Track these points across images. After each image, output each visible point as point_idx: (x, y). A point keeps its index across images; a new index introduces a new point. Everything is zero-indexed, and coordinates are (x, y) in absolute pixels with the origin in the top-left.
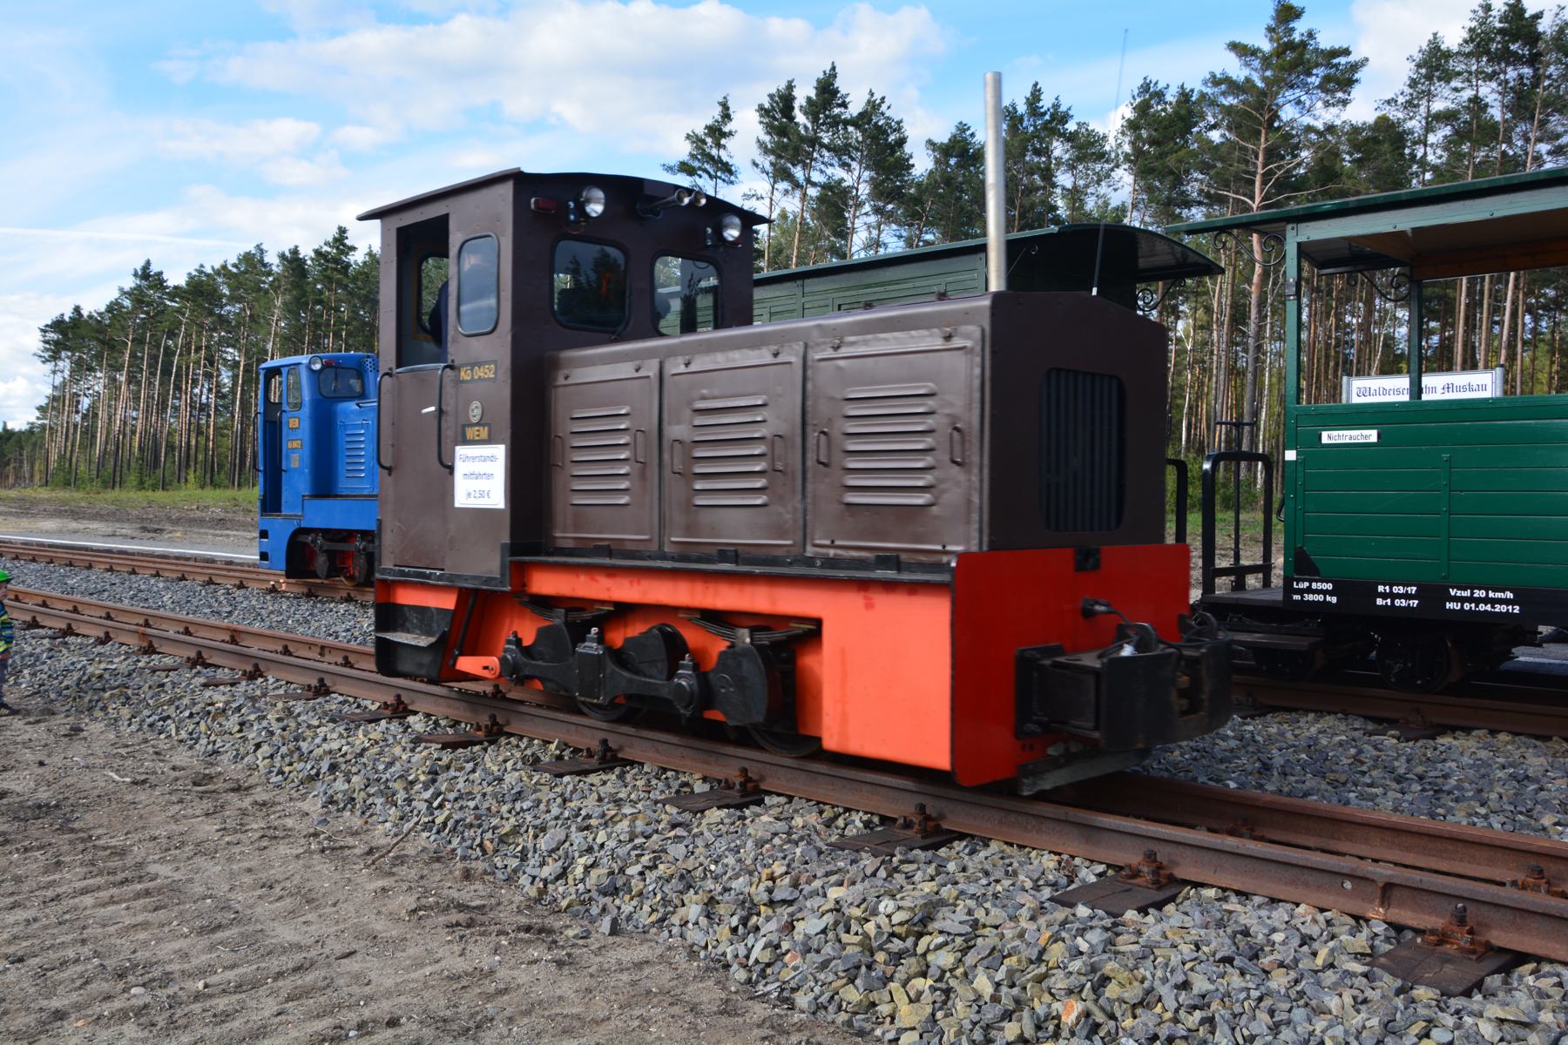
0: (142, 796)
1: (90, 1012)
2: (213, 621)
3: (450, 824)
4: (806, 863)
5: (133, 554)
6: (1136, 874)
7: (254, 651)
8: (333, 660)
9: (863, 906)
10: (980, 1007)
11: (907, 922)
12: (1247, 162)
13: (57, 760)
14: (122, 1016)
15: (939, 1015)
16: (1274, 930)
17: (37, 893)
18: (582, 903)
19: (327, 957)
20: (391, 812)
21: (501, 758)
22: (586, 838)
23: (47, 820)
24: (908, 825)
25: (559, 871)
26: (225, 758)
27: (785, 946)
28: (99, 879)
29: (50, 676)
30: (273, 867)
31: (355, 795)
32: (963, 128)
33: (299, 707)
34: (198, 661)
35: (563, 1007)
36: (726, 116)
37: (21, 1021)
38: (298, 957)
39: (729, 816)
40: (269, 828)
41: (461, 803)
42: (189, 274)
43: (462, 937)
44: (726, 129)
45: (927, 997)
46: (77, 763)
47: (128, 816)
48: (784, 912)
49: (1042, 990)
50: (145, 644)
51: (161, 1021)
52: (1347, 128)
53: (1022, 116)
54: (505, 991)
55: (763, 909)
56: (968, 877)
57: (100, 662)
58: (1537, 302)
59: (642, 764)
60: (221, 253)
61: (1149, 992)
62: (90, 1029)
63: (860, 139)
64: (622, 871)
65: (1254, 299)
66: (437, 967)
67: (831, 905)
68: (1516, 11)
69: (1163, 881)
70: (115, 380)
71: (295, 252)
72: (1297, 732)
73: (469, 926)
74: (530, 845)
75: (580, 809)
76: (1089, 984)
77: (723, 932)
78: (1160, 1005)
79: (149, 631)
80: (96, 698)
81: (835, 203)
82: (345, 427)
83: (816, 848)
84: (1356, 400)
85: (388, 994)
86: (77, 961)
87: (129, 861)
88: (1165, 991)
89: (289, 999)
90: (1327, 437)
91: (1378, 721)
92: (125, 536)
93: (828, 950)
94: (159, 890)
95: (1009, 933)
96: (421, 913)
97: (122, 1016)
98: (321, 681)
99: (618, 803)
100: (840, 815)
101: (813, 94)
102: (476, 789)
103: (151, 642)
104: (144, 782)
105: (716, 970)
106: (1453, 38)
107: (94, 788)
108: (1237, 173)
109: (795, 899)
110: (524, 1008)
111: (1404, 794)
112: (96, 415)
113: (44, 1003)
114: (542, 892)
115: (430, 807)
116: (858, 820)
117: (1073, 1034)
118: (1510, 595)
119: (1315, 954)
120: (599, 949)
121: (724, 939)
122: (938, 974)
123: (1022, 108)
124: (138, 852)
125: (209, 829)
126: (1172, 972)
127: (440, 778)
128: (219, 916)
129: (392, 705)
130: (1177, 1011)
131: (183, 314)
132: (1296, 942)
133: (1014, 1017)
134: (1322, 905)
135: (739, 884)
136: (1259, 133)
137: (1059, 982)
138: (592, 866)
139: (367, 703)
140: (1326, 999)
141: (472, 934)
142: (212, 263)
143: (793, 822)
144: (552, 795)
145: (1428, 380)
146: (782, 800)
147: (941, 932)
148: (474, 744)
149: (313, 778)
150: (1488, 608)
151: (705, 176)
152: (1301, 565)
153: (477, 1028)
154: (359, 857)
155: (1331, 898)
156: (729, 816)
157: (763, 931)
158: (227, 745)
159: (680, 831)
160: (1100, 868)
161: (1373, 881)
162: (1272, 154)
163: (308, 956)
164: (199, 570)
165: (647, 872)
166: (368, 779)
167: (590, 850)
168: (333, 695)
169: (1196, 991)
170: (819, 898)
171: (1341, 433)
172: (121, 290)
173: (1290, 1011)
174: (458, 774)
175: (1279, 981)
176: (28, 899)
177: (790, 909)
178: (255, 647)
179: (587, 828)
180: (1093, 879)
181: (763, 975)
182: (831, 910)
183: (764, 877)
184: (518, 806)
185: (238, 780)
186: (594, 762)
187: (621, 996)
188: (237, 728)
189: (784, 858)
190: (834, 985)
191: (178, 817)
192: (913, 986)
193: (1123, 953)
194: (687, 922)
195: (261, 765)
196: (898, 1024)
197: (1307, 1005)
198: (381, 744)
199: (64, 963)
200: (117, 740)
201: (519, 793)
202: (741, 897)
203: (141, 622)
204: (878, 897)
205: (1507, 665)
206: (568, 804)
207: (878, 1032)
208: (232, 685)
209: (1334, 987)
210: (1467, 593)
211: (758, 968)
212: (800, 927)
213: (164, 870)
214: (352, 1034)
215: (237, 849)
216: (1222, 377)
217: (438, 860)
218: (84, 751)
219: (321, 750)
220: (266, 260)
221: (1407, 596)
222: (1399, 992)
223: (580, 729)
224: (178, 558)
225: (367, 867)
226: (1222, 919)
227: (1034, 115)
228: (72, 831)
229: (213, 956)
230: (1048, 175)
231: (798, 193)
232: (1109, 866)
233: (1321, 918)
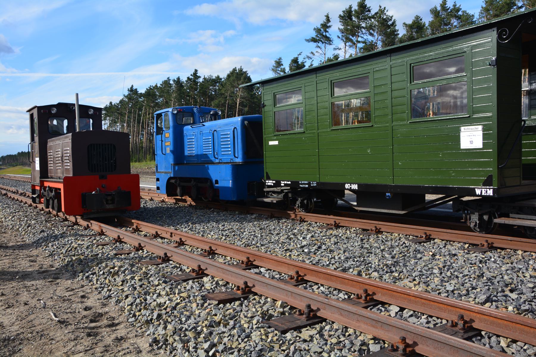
32: (417, 17)
42: (147, 89)
44: (329, 25)
60: (158, 81)
71: (179, 78)
101: (357, 8)
123: (439, 8)
131: (144, 103)
148: (235, 300)
168: (171, 262)
172: (124, 95)
188: (121, 283)
223: (293, 295)
227: (444, 10)
231: (354, 46)
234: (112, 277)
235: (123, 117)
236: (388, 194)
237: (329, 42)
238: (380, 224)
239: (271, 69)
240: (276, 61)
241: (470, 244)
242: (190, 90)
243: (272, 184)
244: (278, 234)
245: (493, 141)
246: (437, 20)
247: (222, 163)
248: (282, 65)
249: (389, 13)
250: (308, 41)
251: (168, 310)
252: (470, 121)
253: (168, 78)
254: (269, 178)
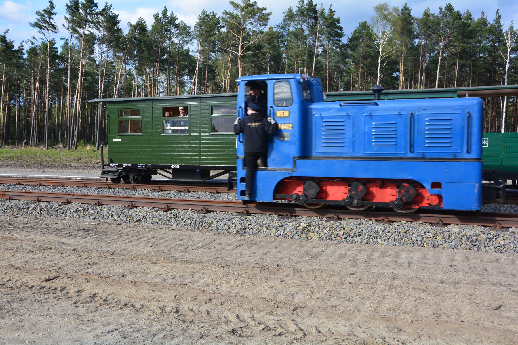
32: (141, 20)
44: (52, 12)
53: (161, 18)
68: (310, 4)
81: (90, 41)
106: (295, 10)
123: (161, 15)
151: (45, 29)
162: (243, 39)
236: (197, 170)
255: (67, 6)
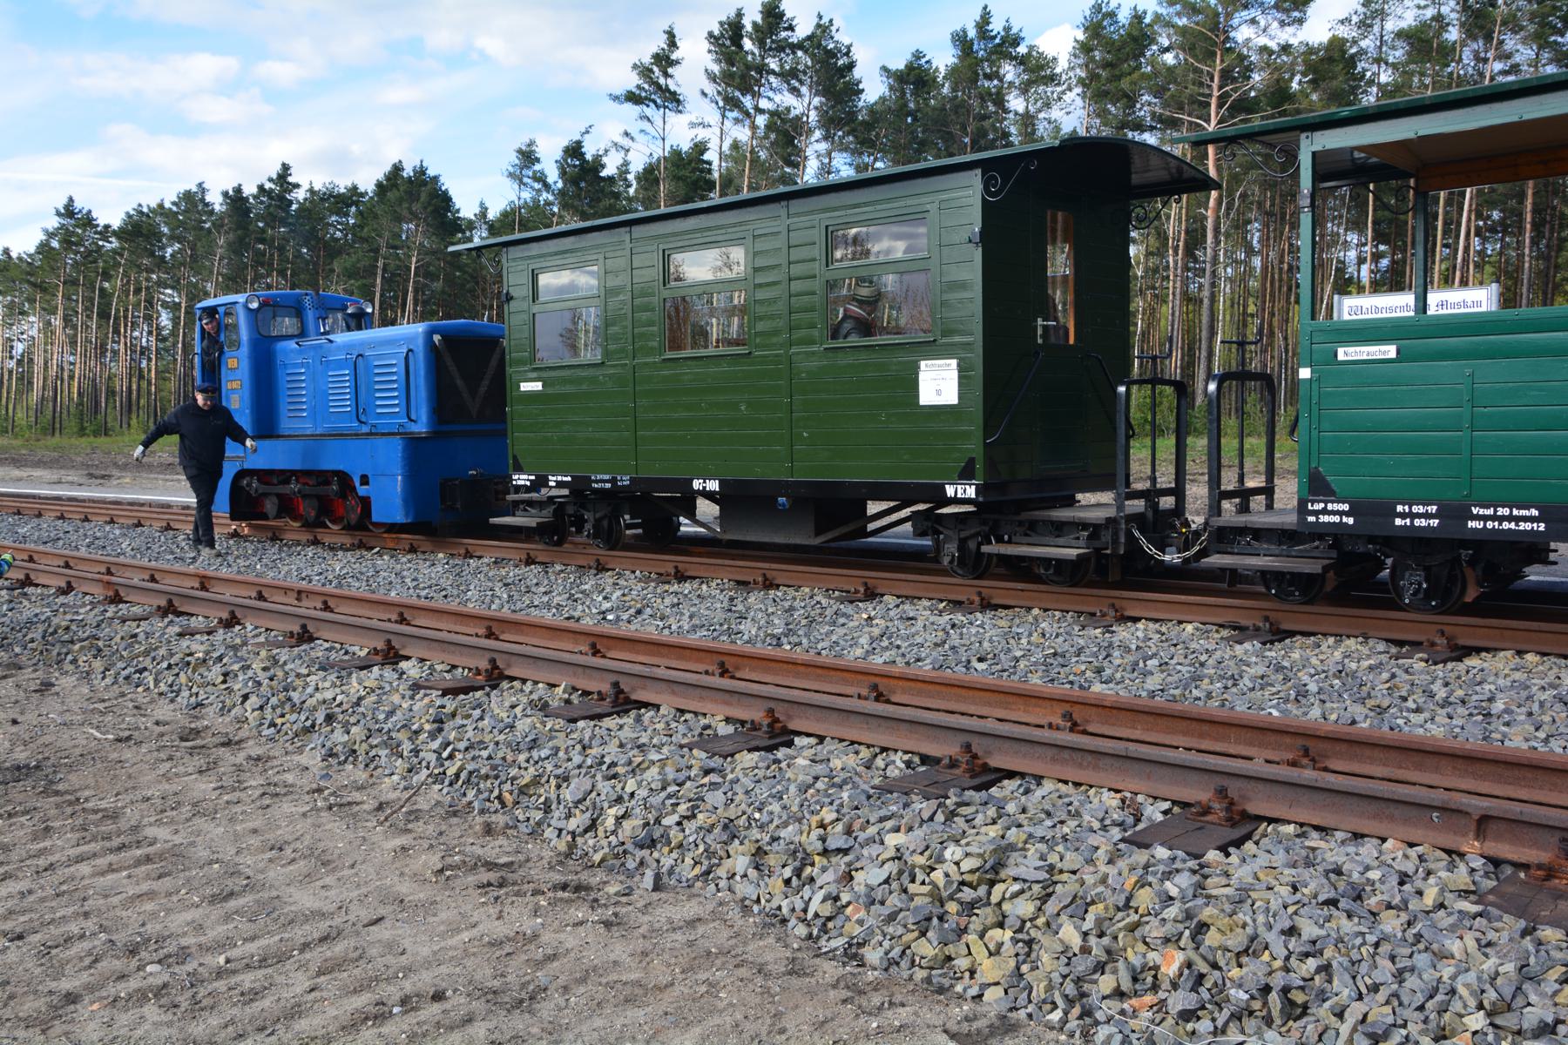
0: (128, 754)
1: (105, 994)
2: (177, 567)
3: (463, 776)
4: (857, 808)
5: (84, 501)
6: (1206, 810)
7: (227, 598)
8: (311, 604)
9: (927, 853)
10: (1069, 959)
11: (978, 869)
12: (1201, 84)
13: (30, 718)
14: (141, 997)
15: (1025, 968)
16: (1368, 868)
17: (28, 862)
18: (617, 856)
19: (354, 924)
20: (397, 764)
21: (507, 704)
22: (614, 787)
23: (29, 783)
24: (953, 764)
25: (588, 822)
26: (210, 711)
27: (845, 898)
28: (93, 845)
29: (12, 629)
30: (279, 827)
31: (356, 747)
32: (918, 55)
33: (284, 654)
34: (169, 610)
35: (620, 973)
36: (672, 44)
37: (30, 1006)
38: (323, 926)
39: (762, 760)
40: (269, 784)
41: (473, 753)
42: (127, 213)
43: (497, 899)
44: (674, 57)
45: (1008, 949)
46: (54, 720)
47: (115, 776)
48: (841, 862)
49: (1136, 940)
50: (111, 593)
51: (184, 1000)
52: (1303, 49)
53: (972, 40)
54: (552, 958)
55: (817, 859)
56: (1031, 819)
57: (65, 613)
58: (1485, 224)
59: (657, 707)
60: (167, 194)
61: (1253, 939)
62: (107, 1012)
63: (809, 63)
64: (658, 821)
65: (1210, 224)
66: (475, 932)
67: (891, 853)
69: (1237, 817)
70: (49, 323)
71: (238, 190)
72: (1321, 657)
73: (501, 886)
74: (553, 796)
75: (603, 756)
76: (1187, 933)
77: (776, 884)
78: (1267, 952)
79: (113, 579)
80: (65, 650)
81: (786, 132)
82: (285, 365)
83: (863, 791)
84: (1346, 317)
85: (427, 964)
86: (82, 936)
87: (123, 824)
88: (1272, 938)
89: (320, 973)
90: (1343, 354)
91: (1400, 643)
92: (72, 483)
93: (894, 901)
94: (161, 856)
95: (1090, 879)
96: (448, 873)
97: (141, 997)
98: (304, 627)
99: (641, 747)
100: (876, 755)
101: (759, 19)
102: (487, 738)
103: (117, 591)
104: (129, 738)
105: (773, 925)
107: (75, 746)
108: (1191, 96)
109: (851, 847)
110: (578, 975)
111: (1451, 718)
112: (31, 361)
113: (53, 985)
114: (572, 846)
115: (439, 758)
116: (899, 759)
117: (1175, 986)
118: (1535, 512)
119: (1420, 893)
120: (645, 906)
121: (777, 891)
122: (1018, 924)
123: (972, 33)
124: (131, 816)
125: (204, 787)
126: (1274, 916)
127: (446, 726)
128: (229, 882)
129: (382, 650)
130: (1287, 958)
131: (121, 255)
132: (1394, 880)
133: (1108, 968)
134: (1411, 839)
135: (788, 833)
136: (1214, 54)
137: (1154, 930)
138: (623, 817)
139: (356, 649)
140: (1447, 942)
141: (507, 894)
142: (150, 201)
143: (831, 765)
144: (570, 743)
145: (1433, 298)
146: (813, 741)
147: (1015, 879)
149: (310, 730)
150: (1513, 526)
152: (1317, 486)
153: (531, 999)
154: (369, 813)
155: (1420, 832)
156: (762, 760)
157: (819, 883)
158: (212, 698)
159: (714, 778)
160: (1166, 805)
161: (1467, 813)
162: (1226, 76)
163: (334, 924)
164: (155, 516)
165: (685, 822)
166: (369, 730)
167: (619, 800)
168: (318, 642)
169: (1305, 937)
170: (876, 846)
171: (1358, 349)
173: (1411, 956)
174: (465, 722)
175: (1391, 924)
176: (19, 869)
177: (847, 859)
178: (227, 593)
179: (615, 776)
180: (1160, 817)
181: (824, 929)
182: (893, 859)
183: (814, 825)
184: (535, 754)
185: (227, 734)
186: (606, 706)
187: (681, 958)
188: (221, 678)
189: (831, 804)
190: (905, 938)
191: (169, 775)
192: (991, 938)
193: (1216, 898)
194: (734, 874)
195: (250, 718)
196: (980, 978)
197: (1427, 949)
198: (378, 692)
199: (68, 940)
200: (92, 694)
201: (534, 740)
202: (792, 847)
203: (103, 570)
204: (941, 843)
205: (1518, 584)
206: (588, 751)
207: (959, 988)
208: (209, 633)
209: (1452, 928)
210: (1490, 512)
211: (819, 922)
212: (859, 877)
213: (162, 833)
214: (395, 1010)
215: (238, 809)
216: (1178, 302)
217: (455, 814)
218: (58, 707)
219: (314, 699)
220: (208, 199)
221: (1427, 516)
222: (1525, 933)
223: (588, 671)
224: (132, 504)
225: (381, 824)
226: (1307, 857)
228: (57, 793)
229: (231, 926)
230: (1000, 101)
231: (747, 122)
232: (1174, 802)
233: (1413, 852)
234: (194, 671)
235: (48, 297)
236: (782, 500)
237: (675, 104)
238: (774, 569)
239: (506, 173)
240: (520, 151)
241: (950, 601)
242: (267, 224)
243: (528, 483)
244: (546, 593)
245: (978, 392)
246: (966, 63)
247: (376, 434)
248: (538, 160)
249: (843, 38)
250: (616, 98)
251: (345, 707)
252: (934, 349)
253: (200, 185)
254: (519, 469)
255: (711, 35)
